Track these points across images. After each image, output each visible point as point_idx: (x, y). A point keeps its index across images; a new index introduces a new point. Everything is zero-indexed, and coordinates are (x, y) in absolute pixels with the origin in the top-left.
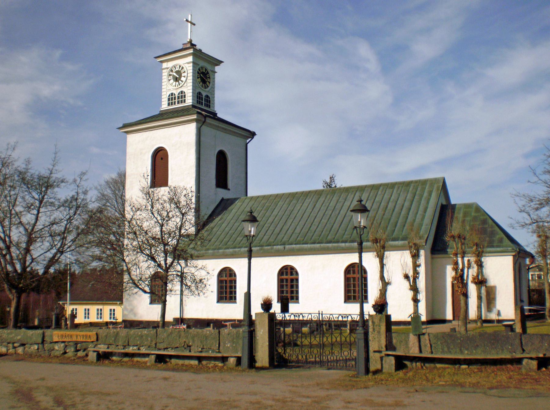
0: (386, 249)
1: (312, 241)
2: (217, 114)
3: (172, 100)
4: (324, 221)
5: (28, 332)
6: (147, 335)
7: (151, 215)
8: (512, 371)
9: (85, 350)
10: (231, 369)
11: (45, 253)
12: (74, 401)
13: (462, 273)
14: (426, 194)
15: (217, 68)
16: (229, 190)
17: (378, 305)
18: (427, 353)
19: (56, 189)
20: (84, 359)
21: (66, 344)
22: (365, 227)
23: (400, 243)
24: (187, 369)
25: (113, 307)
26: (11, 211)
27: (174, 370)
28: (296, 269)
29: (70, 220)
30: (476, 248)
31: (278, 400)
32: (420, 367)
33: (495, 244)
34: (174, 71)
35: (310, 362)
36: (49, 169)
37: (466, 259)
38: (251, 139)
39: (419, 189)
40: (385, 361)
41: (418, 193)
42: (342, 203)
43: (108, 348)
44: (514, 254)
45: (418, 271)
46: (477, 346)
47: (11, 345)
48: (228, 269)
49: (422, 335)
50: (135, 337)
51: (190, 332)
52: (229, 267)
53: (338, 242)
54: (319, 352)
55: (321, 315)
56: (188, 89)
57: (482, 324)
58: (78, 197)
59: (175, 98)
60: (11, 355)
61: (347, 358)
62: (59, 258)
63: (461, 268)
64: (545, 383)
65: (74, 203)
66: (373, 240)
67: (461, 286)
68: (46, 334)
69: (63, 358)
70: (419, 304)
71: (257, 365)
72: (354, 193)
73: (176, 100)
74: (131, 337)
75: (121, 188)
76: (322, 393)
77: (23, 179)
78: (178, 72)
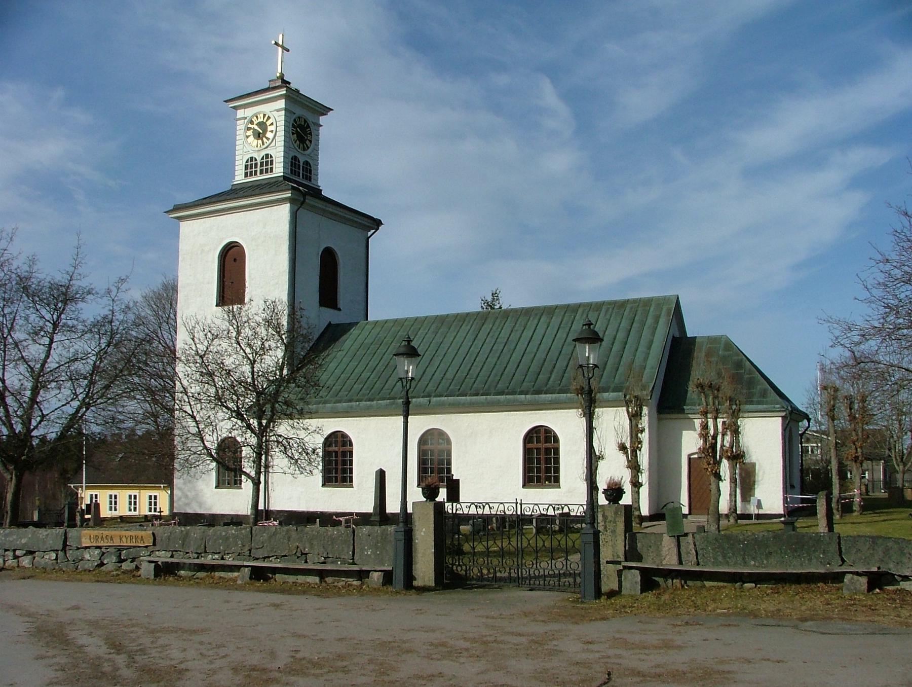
0: (596, 404)
1: (473, 391)
2: (321, 190)
3: (251, 168)
4: (492, 360)
5: (40, 532)
6: (235, 537)
7: (235, 345)
8: (827, 593)
9: (133, 560)
10: (374, 591)
11: (63, 405)
12: (140, 645)
13: (714, 441)
14: (650, 321)
15: (322, 120)
16: (340, 310)
17: (612, 489)
18: (690, 564)
19: (81, 305)
20: (134, 575)
21: (103, 550)
22: (596, 366)
23: (612, 395)
24: (306, 590)
25: (153, 493)
26: (5, 339)
27: (283, 591)
28: (554, 433)
29: (100, 356)
30: (730, 405)
31: (474, 640)
32: (679, 585)
33: (755, 399)
34: (255, 123)
35: (501, 579)
36: (68, 273)
37: (720, 421)
38: (374, 231)
39: (639, 313)
40: (625, 576)
41: (637, 318)
42: (520, 332)
43: (172, 556)
44: (783, 414)
45: (640, 439)
46: (770, 553)
47: (10, 554)
48: (542, 430)
49: (682, 536)
50: (216, 540)
51: (306, 531)
52: (340, 431)
53: (513, 393)
54: (516, 563)
55: (519, 506)
56: (278, 152)
57: (736, 521)
58: (114, 318)
59: (256, 164)
60: (12, 569)
61: (562, 572)
62: (83, 414)
63: (712, 435)
64: (886, 613)
65: (108, 327)
66: (577, 389)
67: (712, 462)
68: (69, 535)
69: (98, 572)
70: (641, 489)
71: (415, 583)
72: (538, 317)
73: (258, 169)
74: (209, 540)
75: (168, 306)
76: (540, 629)
77: (26, 289)
78: (262, 125)
